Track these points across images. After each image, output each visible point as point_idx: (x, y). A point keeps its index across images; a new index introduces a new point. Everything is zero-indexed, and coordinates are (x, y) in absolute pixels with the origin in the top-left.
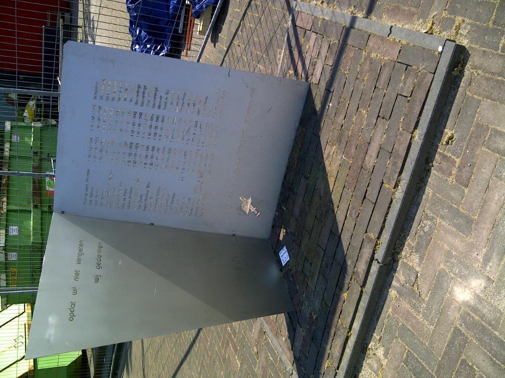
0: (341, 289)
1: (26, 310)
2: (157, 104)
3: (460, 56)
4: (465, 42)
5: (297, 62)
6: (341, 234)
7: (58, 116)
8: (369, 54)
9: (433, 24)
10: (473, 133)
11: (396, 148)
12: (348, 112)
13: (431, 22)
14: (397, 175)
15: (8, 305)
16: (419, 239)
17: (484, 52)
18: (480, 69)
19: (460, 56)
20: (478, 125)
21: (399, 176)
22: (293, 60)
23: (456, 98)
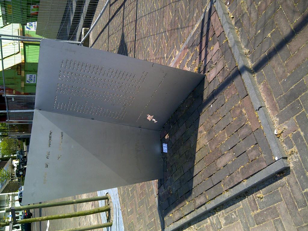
0: (186, 198)
1: (20, 51)
2: (95, 69)
3: (285, 172)
4: (291, 165)
5: (206, 24)
6: (194, 177)
7: (31, 125)
8: (242, 107)
9: (282, 132)
10: (271, 208)
11: (233, 175)
12: (219, 122)
13: (282, 131)
14: (229, 188)
15: (8, 23)
16: (290, 47)
17: (297, 182)
18: (291, 187)
19: (285, 172)
20: (275, 208)
21: (229, 189)
22: (201, 42)
23: (273, 184)
